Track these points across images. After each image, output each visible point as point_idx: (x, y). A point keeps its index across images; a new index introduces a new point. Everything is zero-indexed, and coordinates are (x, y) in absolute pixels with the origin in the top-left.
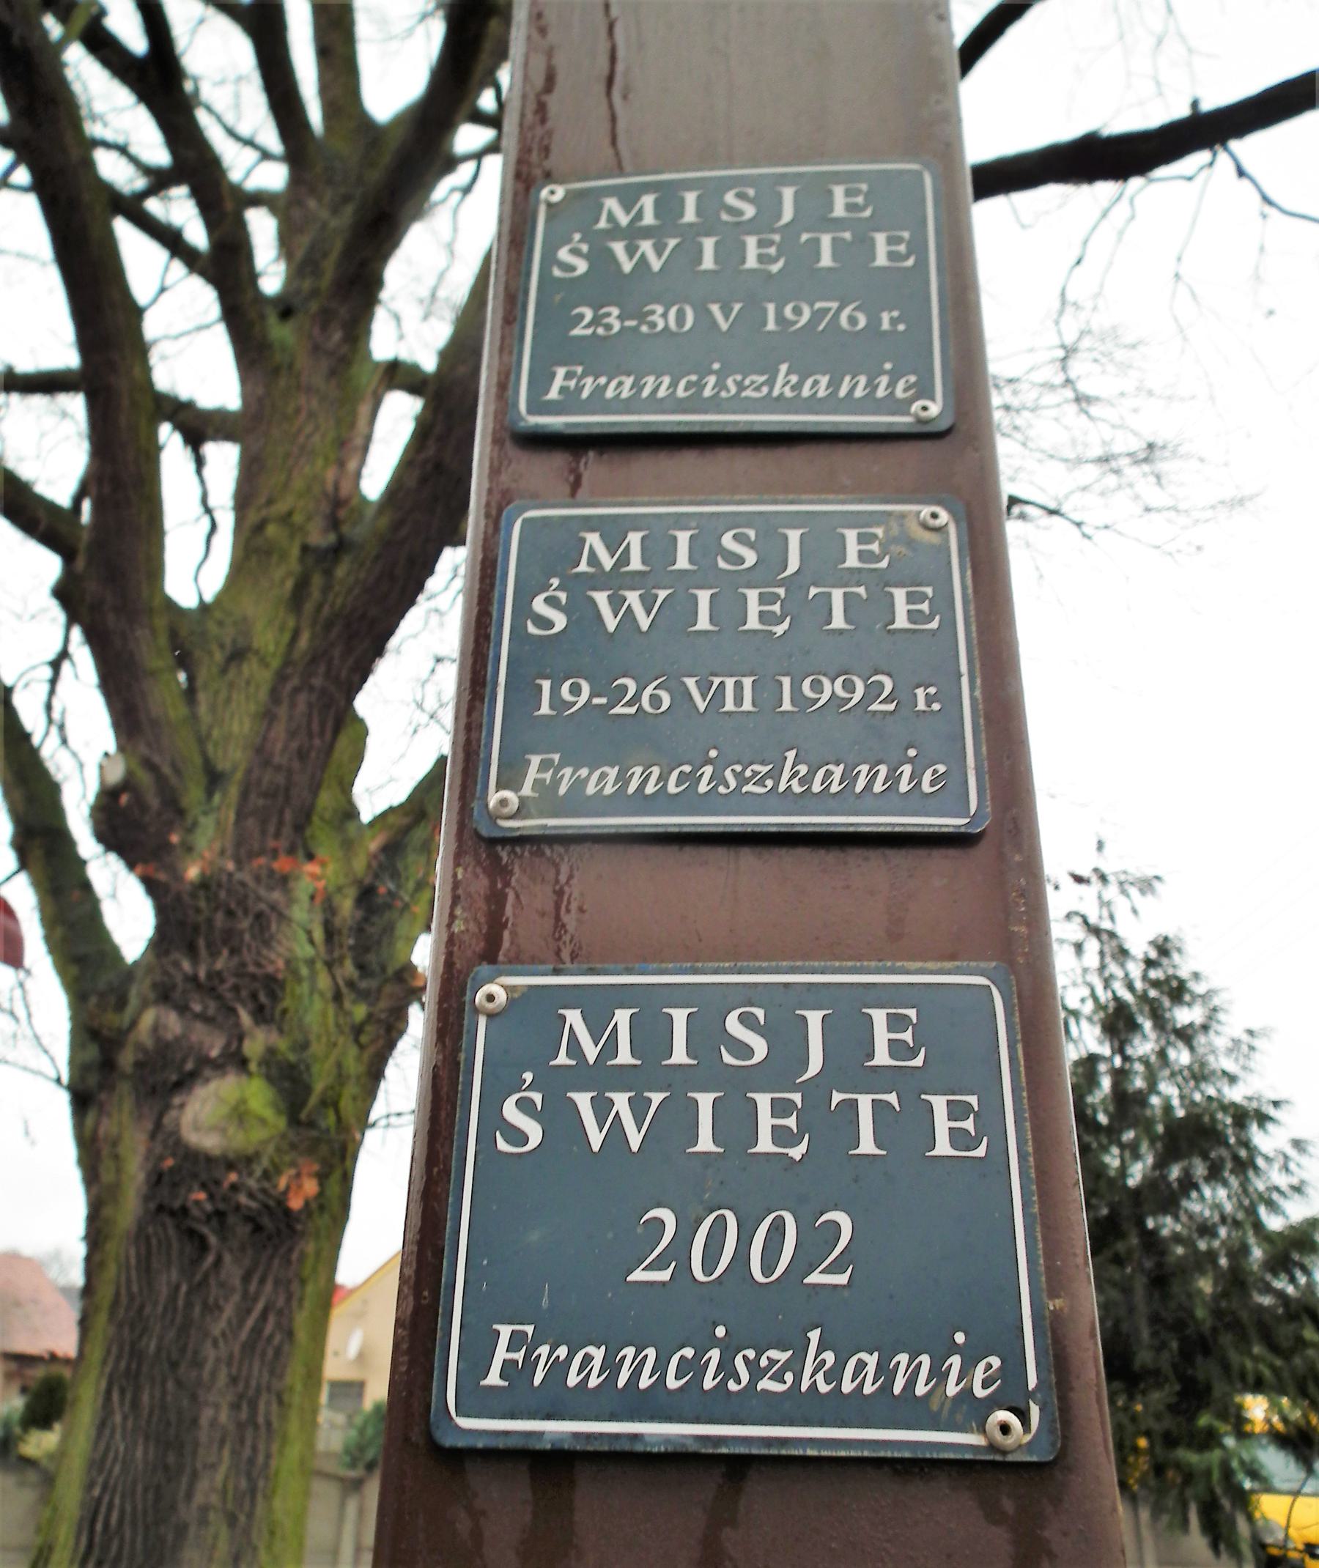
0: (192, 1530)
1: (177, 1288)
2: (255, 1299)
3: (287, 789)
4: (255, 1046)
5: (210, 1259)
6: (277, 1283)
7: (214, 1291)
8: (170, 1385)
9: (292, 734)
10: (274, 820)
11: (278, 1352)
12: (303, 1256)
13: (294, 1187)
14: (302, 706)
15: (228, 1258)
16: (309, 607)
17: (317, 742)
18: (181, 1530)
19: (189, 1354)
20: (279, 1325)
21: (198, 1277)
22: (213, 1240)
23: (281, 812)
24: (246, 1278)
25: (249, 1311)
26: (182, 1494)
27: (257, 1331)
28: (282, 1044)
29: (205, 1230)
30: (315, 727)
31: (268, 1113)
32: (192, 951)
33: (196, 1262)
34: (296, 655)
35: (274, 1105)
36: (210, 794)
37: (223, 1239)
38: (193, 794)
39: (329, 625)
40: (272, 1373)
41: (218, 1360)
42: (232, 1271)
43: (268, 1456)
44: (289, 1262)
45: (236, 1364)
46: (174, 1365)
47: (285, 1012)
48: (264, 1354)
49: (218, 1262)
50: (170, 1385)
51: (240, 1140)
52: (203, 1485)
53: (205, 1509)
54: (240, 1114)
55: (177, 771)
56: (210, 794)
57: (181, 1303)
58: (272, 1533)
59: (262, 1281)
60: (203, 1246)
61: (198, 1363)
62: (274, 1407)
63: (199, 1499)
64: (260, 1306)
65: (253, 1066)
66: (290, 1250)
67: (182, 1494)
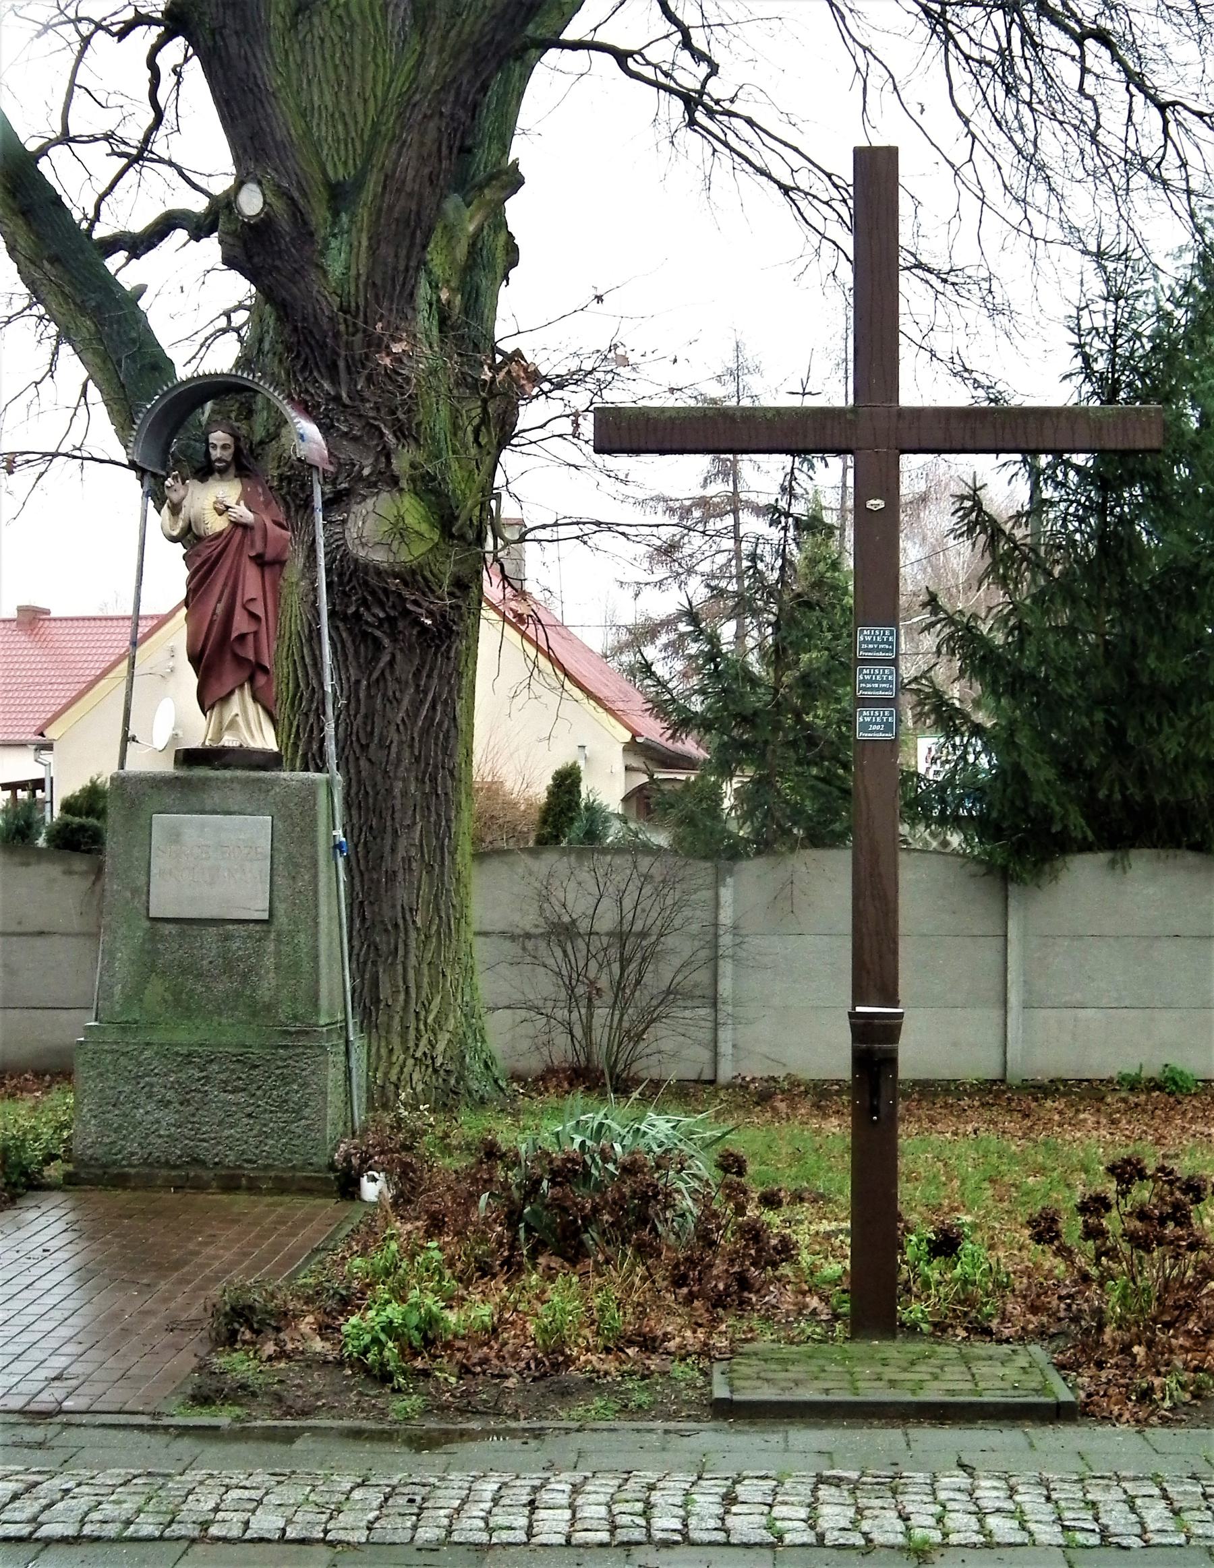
0: (400, 877)
1: (358, 682)
2: (426, 693)
3: (418, 214)
4: (401, 464)
5: (386, 658)
6: (440, 677)
7: (392, 686)
8: (363, 763)
9: (423, 160)
10: (407, 243)
11: (446, 738)
12: (458, 652)
13: (838, 783)
14: (432, 134)
15: (399, 657)
16: (434, 33)
17: (445, 164)
18: (392, 876)
19: (376, 740)
20: (444, 712)
21: (375, 675)
22: (386, 642)
23: (413, 234)
24: (417, 674)
25: (422, 702)
26: (387, 849)
27: (430, 719)
28: (420, 457)
29: (378, 633)
30: (445, 150)
31: (424, 528)
32: (332, 373)
33: (376, 659)
34: (423, 81)
35: (426, 519)
36: (336, 214)
37: (394, 640)
38: (319, 214)
39: (456, 56)
40: (445, 753)
41: (401, 743)
42: (404, 669)
43: (448, 820)
44: (449, 658)
45: (417, 744)
46: (364, 748)
47: (419, 424)
48: (437, 738)
49: (391, 663)
50: (363, 763)
51: (411, 554)
52: (403, 843)
53: (409, 860)
54: (400, 531)
55: (304, 194)
56: (336, 214)
57: (362, 695)
58: (458, 880)
59: (429, 676)
60: (378, 646)
61: (385, 746)
62: (449, 782)
63: (401, 853)
64: (430, 697)
65: (404, 484)
66: (449, 648)
67: (387, 849)
